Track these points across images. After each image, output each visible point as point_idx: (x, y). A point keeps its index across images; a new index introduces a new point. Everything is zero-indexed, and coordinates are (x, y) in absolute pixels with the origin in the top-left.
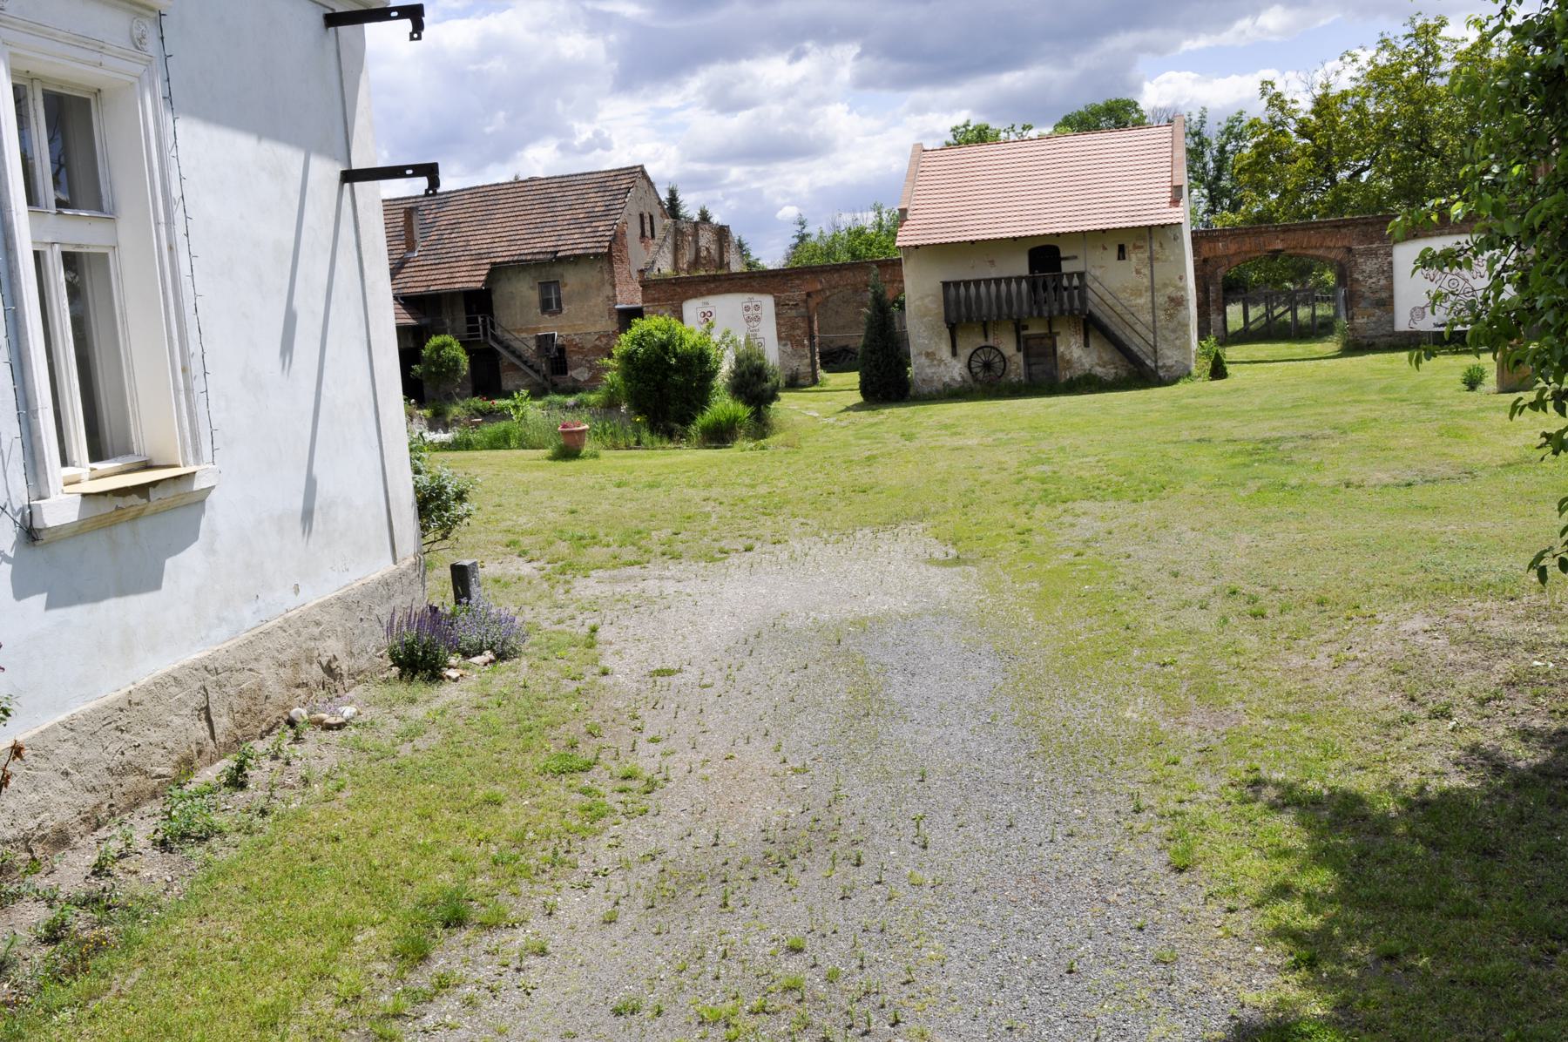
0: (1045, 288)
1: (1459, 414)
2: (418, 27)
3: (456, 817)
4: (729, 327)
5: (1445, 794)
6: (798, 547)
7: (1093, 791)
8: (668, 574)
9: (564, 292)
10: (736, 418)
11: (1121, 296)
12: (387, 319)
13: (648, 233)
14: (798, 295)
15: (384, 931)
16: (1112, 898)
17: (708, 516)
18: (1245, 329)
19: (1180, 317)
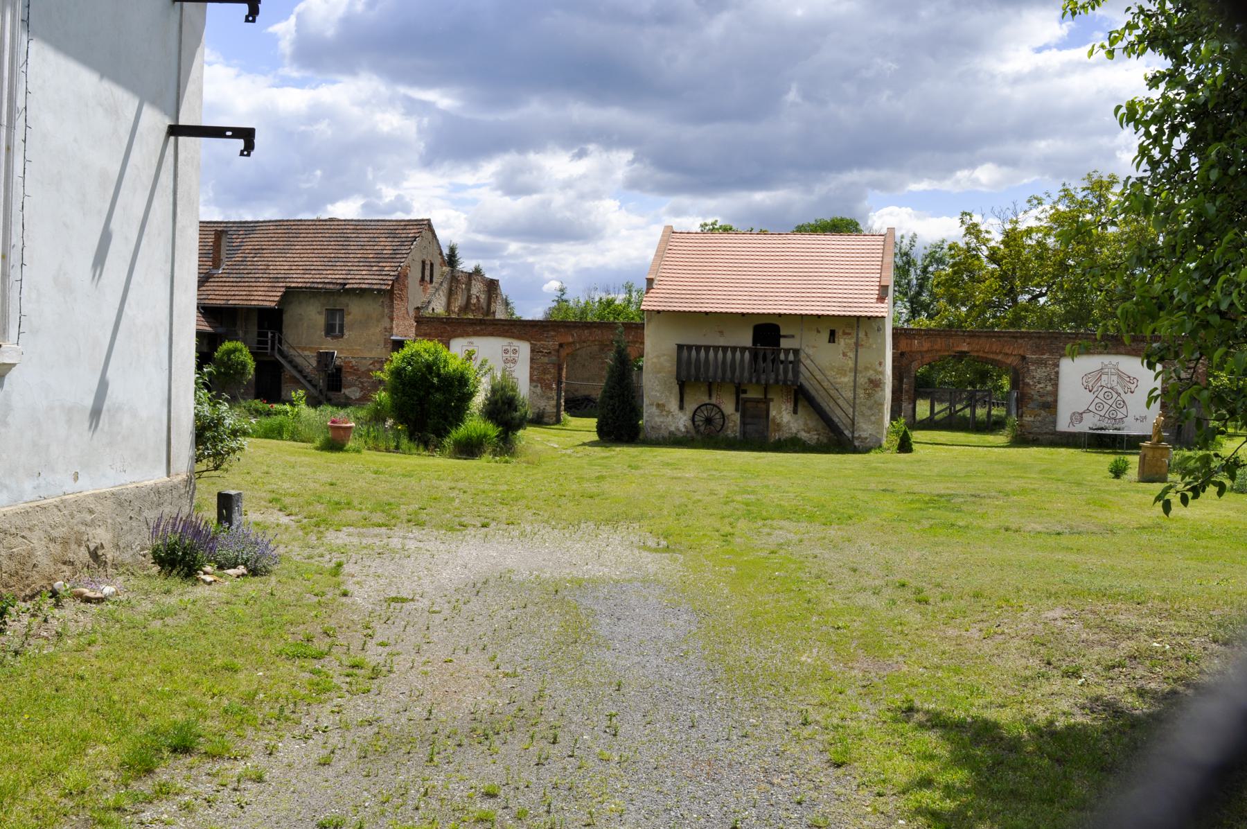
0: (765, 360)
1: (1105, 491)
2: (249, 147)
3: (194, 676)
4: (490, 363)
5: (1070, 728)
6: (529, 529)
7: (767, 708)
8: (410, 535)
9: (347, 319)
10: (485, 436)
11: (828, 373)
12: (189, 325)
13: (427, 278)
14: (552, 344)
15: (116, 747)
16: (776, 781)
17: (453, 499)
18: (931, 419)
19: (877, 396)
